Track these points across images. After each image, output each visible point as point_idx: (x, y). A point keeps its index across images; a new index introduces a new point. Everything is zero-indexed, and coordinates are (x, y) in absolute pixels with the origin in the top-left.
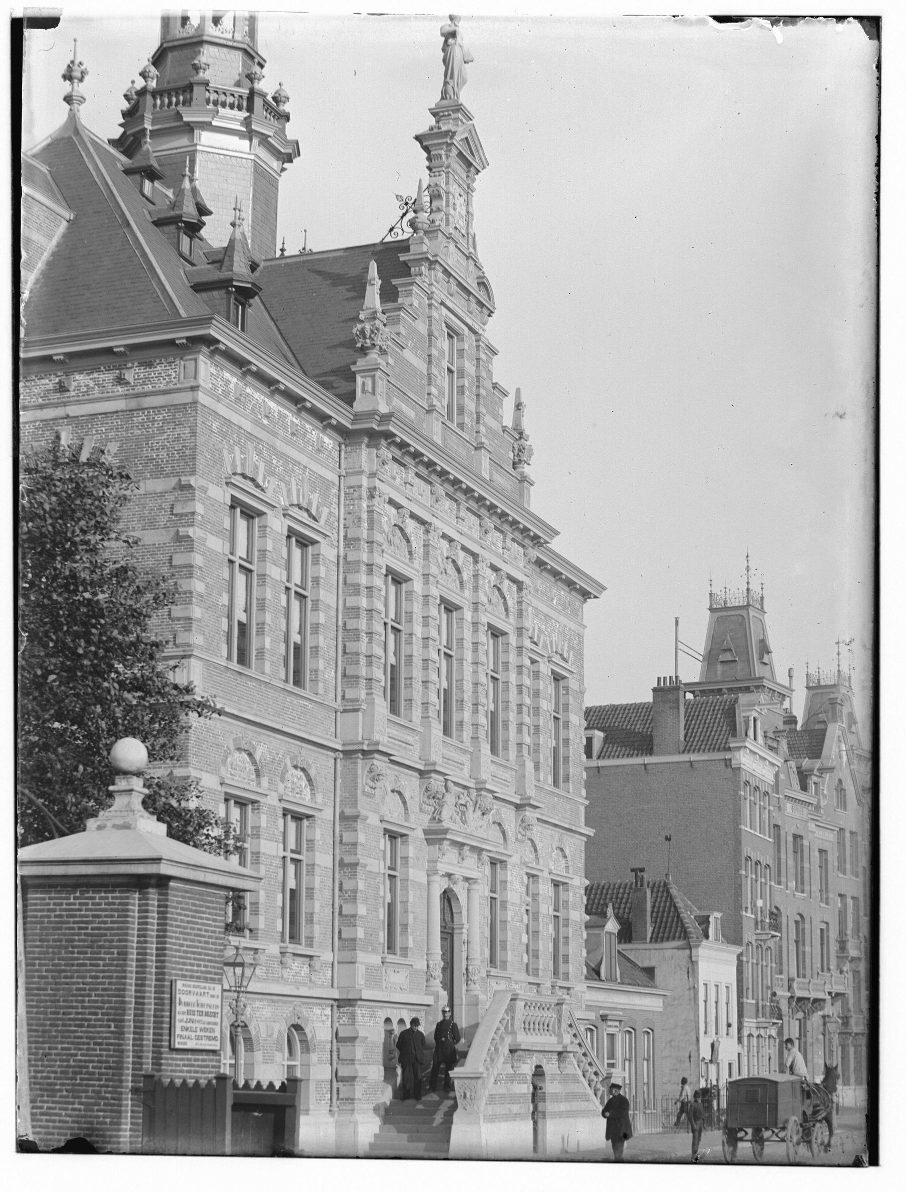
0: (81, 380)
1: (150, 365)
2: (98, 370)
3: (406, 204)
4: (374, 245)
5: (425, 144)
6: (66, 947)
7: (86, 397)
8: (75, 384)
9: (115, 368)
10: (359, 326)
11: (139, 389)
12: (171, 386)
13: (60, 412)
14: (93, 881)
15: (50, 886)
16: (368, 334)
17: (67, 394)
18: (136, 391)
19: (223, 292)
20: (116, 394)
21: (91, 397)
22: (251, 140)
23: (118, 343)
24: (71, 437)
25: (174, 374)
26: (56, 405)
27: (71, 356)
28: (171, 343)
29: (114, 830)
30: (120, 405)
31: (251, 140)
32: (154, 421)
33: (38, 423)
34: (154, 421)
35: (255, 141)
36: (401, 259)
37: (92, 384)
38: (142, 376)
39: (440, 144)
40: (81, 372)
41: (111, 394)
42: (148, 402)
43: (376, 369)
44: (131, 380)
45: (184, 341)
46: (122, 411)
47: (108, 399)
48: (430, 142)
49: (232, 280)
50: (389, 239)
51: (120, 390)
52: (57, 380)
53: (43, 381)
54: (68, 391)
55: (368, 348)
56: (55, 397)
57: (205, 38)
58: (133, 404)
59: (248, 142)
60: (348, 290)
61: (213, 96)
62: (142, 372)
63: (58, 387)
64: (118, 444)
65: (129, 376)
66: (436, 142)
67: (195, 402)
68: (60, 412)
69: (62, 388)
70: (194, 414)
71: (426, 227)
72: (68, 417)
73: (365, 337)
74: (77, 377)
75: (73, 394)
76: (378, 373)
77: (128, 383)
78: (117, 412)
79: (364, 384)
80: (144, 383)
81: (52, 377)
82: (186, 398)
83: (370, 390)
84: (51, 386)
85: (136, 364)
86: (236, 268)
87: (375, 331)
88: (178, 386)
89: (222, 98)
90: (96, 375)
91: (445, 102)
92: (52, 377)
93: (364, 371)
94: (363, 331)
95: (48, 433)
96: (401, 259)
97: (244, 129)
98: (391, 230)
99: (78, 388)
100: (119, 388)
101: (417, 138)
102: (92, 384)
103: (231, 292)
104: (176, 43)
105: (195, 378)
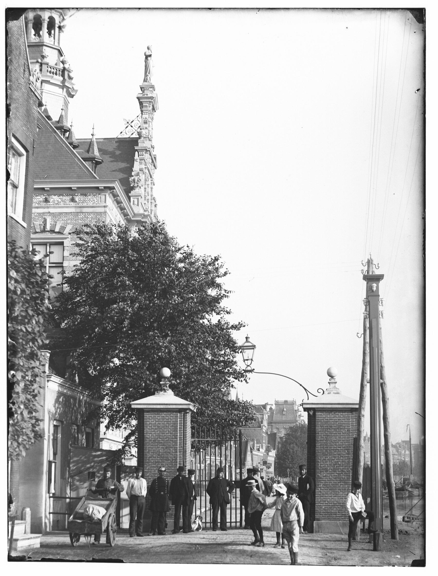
0: (54, 199)
1: (86, 195)
2: (63, 195)
3: (128, 123)
4: (114, 138)
5: (141, 101)
6: (330, 428)
7: (57, 206)
8: (53, 200)
9: (70, 195)
10: (132, 178)
11: (81, 205)
12: (95, 205)
13: (46, 210)
14: (338, 409)
15: (323, 411)
16: (136, 181)
17: (49, 203)
18: (79, 205)
19: (90, 162)
20: (71, 205)
21: (59, 206)
22: (63, 89)
23: (74, 186)
24: (51, 221)
25: (96, 200)
26: (44, 208)
27: (51, 188)
28: (97, 188)
29: (334, 394)
30: (73, 210)
31: (63, 89)
32: (87, 218)
33: (36, 214)
34: (87, 218)
35: (65, 90)
36: (136, 148)
37: (60, 200)
38: (82, 199)
39: (147, 101)
40: (55, 195)
41: (68, 205)
42: (85, 210)
43: (139, 196)
44: (77, 201)
45: (103, 188)
46: (74, 213)
47: (67, 207)
48: (143, 100)
49: (95, 158)
50: (120, 137)
51: (73, 204)
52: (44, 197)
53: (38, 197)
54: (49, 202)
55: (135, 187)
56: (43, 204)
57: (45, 44)
58: (78, 210)
59: (62, 90)
60: (110, 157)
61: (49, 69)
62: (82, 198)
63: (44, 200)
64: (72, 226)
65: (77, 199)
66: (146, 100)
67: (106, 212)
68: (46, 210)
69: (46, 201)
70: (105, 216)
71: (145, 136)
72: (49, 213)
73: (135, 183)
74: (53, 197)
75: (51, 203)
76: (140, 198)
77: (76, 202)
78: (71, 213)
79: (134, 201)
80: (83, 202)
81: (42, 196)
82: (102, 210)
83: (136, 204)
84: (41, 200)
85: (79, 194)
86: (95, 153)
87: (139, 180)
88: (98, 205)
89: (52, 70)
90: (61, 197)
91: (146, 83)
92: (42, 196)
93: (133, 196)
94: (134, 180)
95: (40, 218)
96: (136, 148)
97: (61, 85)
98: (121, 133)
99: (54, 201)
100: (72, 203)
101: (138, 98)
102: (60, 200)
103: (94, 163)
104: (32, 44)
105: (105, 202)
